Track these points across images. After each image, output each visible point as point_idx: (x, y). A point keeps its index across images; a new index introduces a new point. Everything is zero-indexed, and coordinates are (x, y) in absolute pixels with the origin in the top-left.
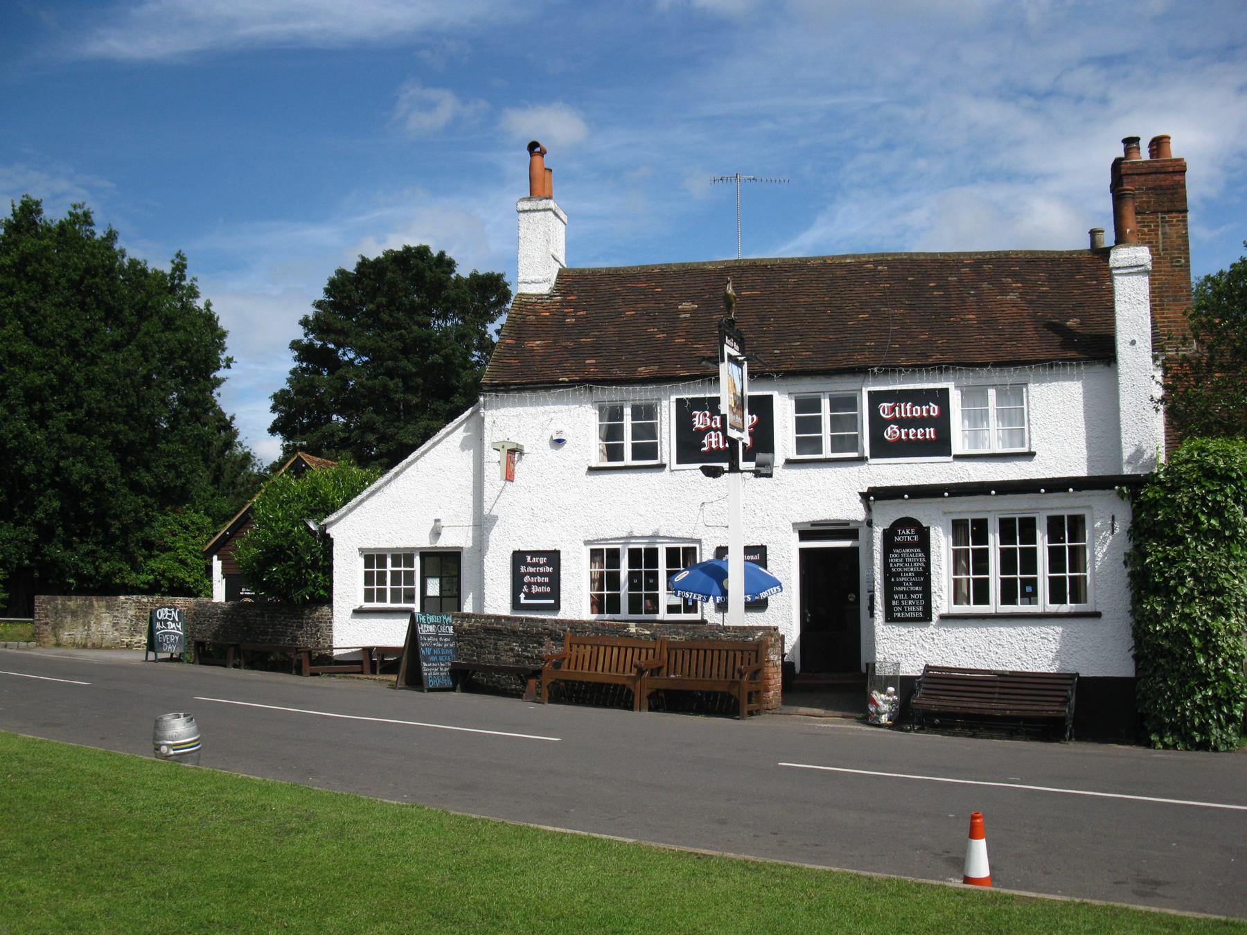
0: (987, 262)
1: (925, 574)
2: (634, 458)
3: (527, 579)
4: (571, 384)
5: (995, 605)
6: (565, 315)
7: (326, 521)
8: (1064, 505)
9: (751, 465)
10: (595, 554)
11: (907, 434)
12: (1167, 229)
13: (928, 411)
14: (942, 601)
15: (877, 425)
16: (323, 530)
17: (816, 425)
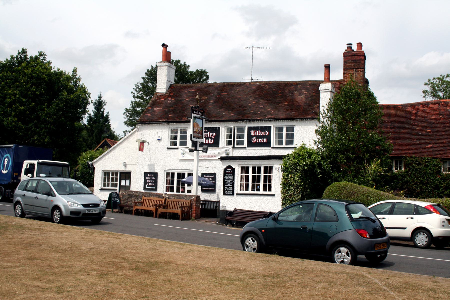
0: (300, 84)
1: (233, 182)
2: (286, 145)
3: (148, 181)
4: (163, 122)
5: (250, 191)
6: (168, 100)
7: (93, 161)
8: (267, 163)
9: (201, 149)
10: (168, 174)
11: (258, 140)
12: (357, 74)
13: (265, 133)
14: (237, 189)
15: (250, 137)
16: (92, 164)
17: (287, 136)
